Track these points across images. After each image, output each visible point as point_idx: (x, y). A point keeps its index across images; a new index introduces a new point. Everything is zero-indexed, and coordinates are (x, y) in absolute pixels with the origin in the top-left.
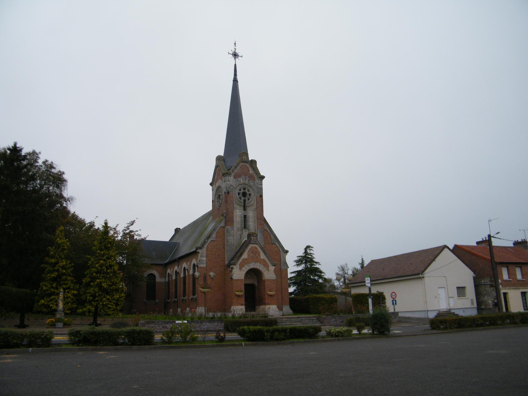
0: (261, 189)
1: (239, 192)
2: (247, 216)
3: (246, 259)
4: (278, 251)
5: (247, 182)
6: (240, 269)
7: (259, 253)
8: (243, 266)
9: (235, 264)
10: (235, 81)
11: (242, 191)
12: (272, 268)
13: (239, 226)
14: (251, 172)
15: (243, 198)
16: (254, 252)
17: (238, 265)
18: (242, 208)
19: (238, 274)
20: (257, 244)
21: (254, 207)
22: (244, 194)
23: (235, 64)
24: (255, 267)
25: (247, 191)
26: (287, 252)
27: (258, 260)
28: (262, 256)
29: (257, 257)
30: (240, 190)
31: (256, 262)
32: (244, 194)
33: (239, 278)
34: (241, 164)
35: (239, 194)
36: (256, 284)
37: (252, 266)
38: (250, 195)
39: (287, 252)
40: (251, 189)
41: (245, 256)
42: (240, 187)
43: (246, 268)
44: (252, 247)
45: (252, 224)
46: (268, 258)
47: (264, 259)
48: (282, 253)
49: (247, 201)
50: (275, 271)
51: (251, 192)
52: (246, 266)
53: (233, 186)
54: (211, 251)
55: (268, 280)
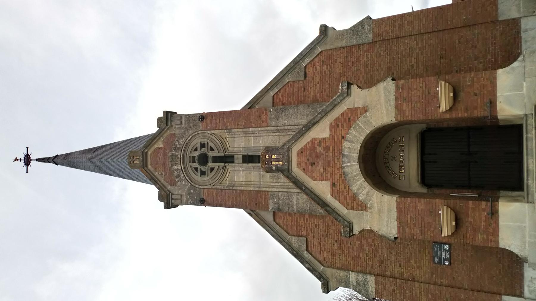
0: (189, 116)
1: (199, 174)
2: (245, 154)
3: (333, 185)
4: (322, 58)
5: (178, 154)
6: (363, 207)
7: (313, 141)
8: (354, 197)
9: (350, 226)
10: (55, 160)
11: (196, 165)
12: (358, 97)
14: (160, 144)
15: (211, 164)
17: (351, 215)
18: (229, 166)
19: (380, 214)
20: (289, 150)
21: (225, 134)
22: (203, 159)
24: (356, 155)
25: (196, 154)
26: (324, 30)
27: (334, 146)
28: (322, 131)
29: (327, 148)
30: (196, 169)
31: (340, 153)
33: (394, 214)
34: (150, 167)
35: (203, 173)
36: (416, 130)
37: (353, 167)
38: (203, 146)
39: (324, 30)
40: (193, 143)
41: (323, 189)
43: (361, 186)
44: (299, 165)
45: (260, 141)
46: (326, 113)
47: (332, 127)
48: (329, 45)
49: (216, 153)
50: (369, 83)
51: (196, 142)
52: (355, 188)
53: (189, 190)
54: (334, 255)
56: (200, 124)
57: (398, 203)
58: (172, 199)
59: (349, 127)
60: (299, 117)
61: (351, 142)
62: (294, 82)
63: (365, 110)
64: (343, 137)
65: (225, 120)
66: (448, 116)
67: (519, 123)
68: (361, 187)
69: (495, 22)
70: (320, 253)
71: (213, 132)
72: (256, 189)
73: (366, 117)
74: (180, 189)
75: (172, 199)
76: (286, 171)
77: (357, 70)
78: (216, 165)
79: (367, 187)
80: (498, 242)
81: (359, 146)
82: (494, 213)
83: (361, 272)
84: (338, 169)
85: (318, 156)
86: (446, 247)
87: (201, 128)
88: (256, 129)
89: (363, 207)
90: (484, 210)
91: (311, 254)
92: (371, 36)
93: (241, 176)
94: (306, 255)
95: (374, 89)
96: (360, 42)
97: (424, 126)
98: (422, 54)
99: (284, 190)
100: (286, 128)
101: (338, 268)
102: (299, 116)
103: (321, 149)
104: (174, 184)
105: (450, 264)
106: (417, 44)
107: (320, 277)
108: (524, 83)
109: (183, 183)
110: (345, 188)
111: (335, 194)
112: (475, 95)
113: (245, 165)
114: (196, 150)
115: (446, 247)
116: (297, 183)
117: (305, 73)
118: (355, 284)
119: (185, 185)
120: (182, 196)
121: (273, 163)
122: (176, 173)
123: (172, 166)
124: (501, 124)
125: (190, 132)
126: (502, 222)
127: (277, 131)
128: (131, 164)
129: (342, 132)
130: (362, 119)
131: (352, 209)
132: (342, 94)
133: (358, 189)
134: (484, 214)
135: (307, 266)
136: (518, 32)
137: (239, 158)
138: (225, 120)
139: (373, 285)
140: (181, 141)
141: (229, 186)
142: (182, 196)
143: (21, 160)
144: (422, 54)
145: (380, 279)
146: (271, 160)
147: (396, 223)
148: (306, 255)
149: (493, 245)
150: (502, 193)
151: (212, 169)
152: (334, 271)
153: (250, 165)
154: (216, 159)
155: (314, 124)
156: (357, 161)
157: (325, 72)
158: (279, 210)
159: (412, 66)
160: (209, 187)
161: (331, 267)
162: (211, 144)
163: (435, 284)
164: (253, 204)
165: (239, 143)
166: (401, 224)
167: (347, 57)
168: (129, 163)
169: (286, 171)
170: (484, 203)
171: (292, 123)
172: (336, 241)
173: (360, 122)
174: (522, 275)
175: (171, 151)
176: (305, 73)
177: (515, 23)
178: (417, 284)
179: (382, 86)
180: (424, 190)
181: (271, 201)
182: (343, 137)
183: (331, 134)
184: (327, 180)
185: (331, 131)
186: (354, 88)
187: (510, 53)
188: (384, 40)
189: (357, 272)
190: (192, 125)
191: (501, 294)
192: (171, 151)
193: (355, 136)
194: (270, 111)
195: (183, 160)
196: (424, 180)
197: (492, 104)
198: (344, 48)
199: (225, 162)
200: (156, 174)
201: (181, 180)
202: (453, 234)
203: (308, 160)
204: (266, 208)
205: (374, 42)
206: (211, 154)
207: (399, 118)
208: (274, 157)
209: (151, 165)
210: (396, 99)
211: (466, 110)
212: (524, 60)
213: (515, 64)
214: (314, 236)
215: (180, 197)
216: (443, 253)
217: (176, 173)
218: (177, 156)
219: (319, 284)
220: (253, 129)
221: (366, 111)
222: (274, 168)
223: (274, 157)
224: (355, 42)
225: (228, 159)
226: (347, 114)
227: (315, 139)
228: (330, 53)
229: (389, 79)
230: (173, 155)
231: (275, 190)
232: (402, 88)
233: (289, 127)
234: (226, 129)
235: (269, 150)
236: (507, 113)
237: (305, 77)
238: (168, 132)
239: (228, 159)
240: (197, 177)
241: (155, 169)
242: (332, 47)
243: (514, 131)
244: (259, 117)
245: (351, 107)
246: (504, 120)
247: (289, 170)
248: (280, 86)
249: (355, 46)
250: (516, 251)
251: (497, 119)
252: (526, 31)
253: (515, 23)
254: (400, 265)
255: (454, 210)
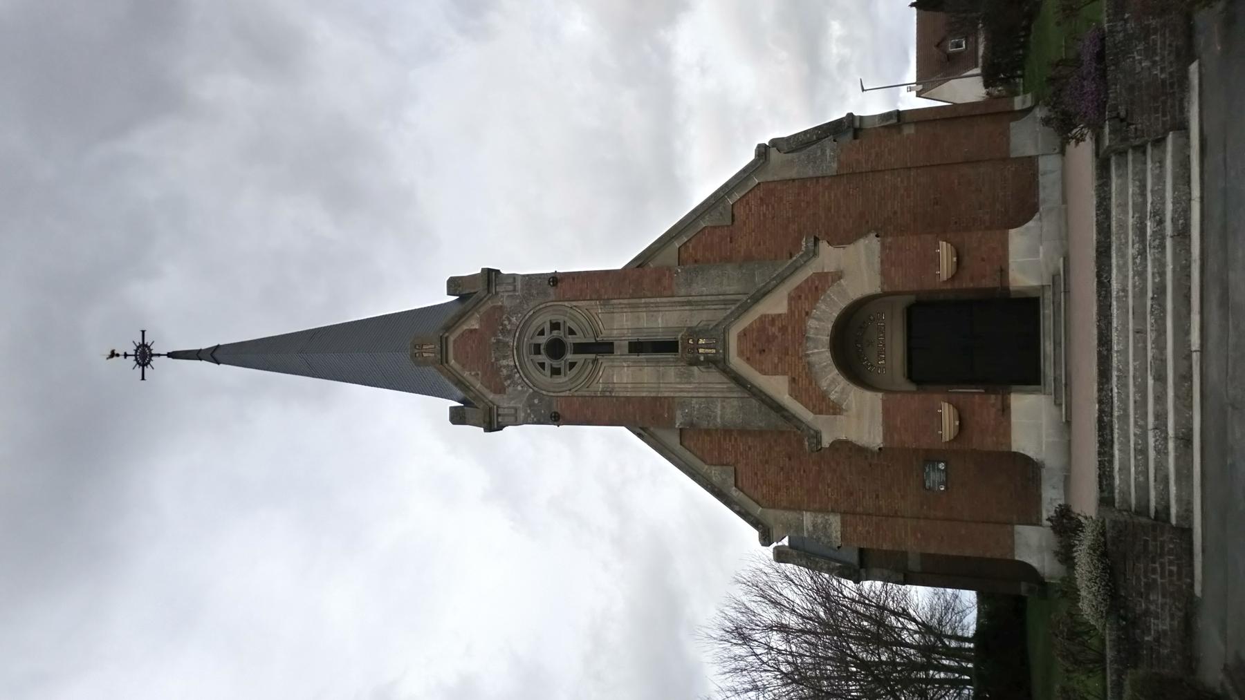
0: (529, 279)
1: (548, 372)
2: (634, 338)
3: (793, 380)
4: (760, 193)
5: (509, 339)
6: (835, 409)
7: (763, 318)
8: (824, 396)
9: (817, 436)
10: (215, 355)
11: (543, 358)
12: (829, 257)
13: (671, 373)
15: (570, 357)
16: (761, 343)
18: (604, 360)
19: (861, 418)
20: (725, 331)
21: (598, 310)
22: (556, 349)
23: (170, 355)
24: (826, 339)
25: (543, 340)
28: (776, 305)
29: (783, 329)
30: (542, 365)
31: (802, 336)
32: (556, 349)
33: (879, 418)
34: (452, 362)
35: (556, 372)
36: (902, 303)
37: (821, 355)
38: (555, 326)
41: (777, 387)
42: (530, 367)
43: (833, 381)
44: (741, 353)
45: (662, 320)
46: (782, 279)
49: (579, 338)
50: (842, 239)
51: (544, 320)
52: (824, 385)
53: (532, 397)
55: (884, 274)
56: (551, 290)
57: (884, 401)
58: (498, 415)
59: (816, 300)
60: (730, 283)
61: (818, 319)
62: (715, 227)
63: (838, 275)
64: (807, 314)
65: (597, 285)
66: (949, 287)
67: (1034, 295)
68: (833, 381)
69: (1006, 159)
70: (756, 488)
71: (574, 303)
72: (653, 395)
73: (839, 285)
74: (513, 399)
75: (498, 415)
76: (719, 363)
77: (814, 214)
78: (580, 358)
79: (842, 382)
80: (1010, 445)
81: (830, 326)
82: (1005, 410)
83: (820, 511)
84: (800, 358)
85: (770, 339)
86: (942, 466)
87: (552, 298)
88: (652, 300)
89: (835, 409)
90: (993, 405)
91: (742, 490)
92: (835, 165)
93: (625, 376)
94: (735, 493)
95: (851, 248)
96: (819, 174)
97: (912, 298)
98: (909, 196)
99: (700, 395)
100: (704, 298)
101: (785, 508)
102: (725, 281)
103: (774, 330)
104: (501, 390)
105: (947, 488)
106: (902, 182)
107: (755, 523)
108: (1041, 248)
109: (519, 388)
110: (810, 383)
111: (795, 394)
112: (983, 260)
113: (634, 357)
114: (542, 333)
115: (942, 466)
116: (738, 380)
117: (733, 215)
118: (811, 529)
119: (522, 392)
120: (516, 410)
121: (701, 351)
122: (505, 372)
123: (497, 360)
124: (1013, 296)
125: (532, 304)
126: (1014, 419)
127: (689, 303)
128: (418, 360)
129: (807, 307)
130: (835, 288)
131: (821, 413)
132: (806, 253)
133: (829, 385)
134: (993, 410)
135: (737, 508)
136: (1035, 175)
137: (622, 347)
138: (597, 285)
139: (839, 528)
140: (514, 319)
141: (603, 391)
142: (516, 410)
143: (126, 355)
144: (909, 196)
145: (849, 518)
146: (697, 346)
147: (881, 429)
148: (735, 493)
149: (1004, 448)
150: (1015, 387)
151: (572, 365)
152: (779, 513)
153: (642, 356)
154: (580, 348)
155: (765, 294)
156: (828, 346)
157: (764, 215)
158: (692, 425)
159: (895, 213)
160: (567, 393)
161: (774, 507)
162: (570, 324)
163: (926, 518)
164: (648, 420)
165: (622, 323)
166: (889, 429)
167: (799, 194)
168: (413, 356)
169: (719, 363)
170: (993, 396)
171: (714, 291)
172: (782, 469)
173: (832, 292)
174: (1040, 496)
175: (495, 335)
176: (733, 215)
177: (1031, 162)
178: (901, 521)
179: (862, 243)
180: (913, 387)
181: (678, 413)
182: (807, 314)
183: (790, 309)
184: (784, 373)
185: (790, 304)
186: (823, 245)
187: (1023, 208)
188: (854, 173)
189: (815, 511)
190: (535, 292)
191: (1012, 524)
192: (495, 335)
193: (824, 311)
194: (677, 272)
195: (502, 351)
196: (911, 376)
197: (1003, 271)
198: (794, 180)
199: (597, 353)
200: (466, 374)
201: (515, 384)
202: (955, 438)
203: (754, 345)
204: (670, 424)
205: (839, 176)
206: (570, 340)
207: (886, 288)
208: (701, 342)
209: (455, 359)
210: (882, 262)
211: (972, 279)
212: (1040, 219)
213: (1031, 224)
214: (747, 464)
215: (513, 411)
216: (938, 475)
217: (505, 372)
218: (506, 345)
219: (754, 534)
220: (647, 300)
221: (840, 278)
222: (702, 358)
223: (701, 342)
224: (811, 174)
225: (605, 348)
226: (813, 282)
227: (765, 316)
228: (772, 186)
229: (873, 235)
230: (498, 341)
231: (686, 394)
232: (890, 248)
233: (709, 298)
234: (599, 299)
235: (694, 333)
236: (1022, 284)
237: (733, 220)
238: (490, 304)
239: (605, 348)
240: (544, 378)
241: (463, 366)
242: (776, 178)
243: (1028, 305)
244: (659, 281)
245: (820, 271)
246: (1018, 292)
247: (725, 360)
248: (691, 234)
249: (811, 178)
250: (1031, 454)
251: (1007, 289)
252: (1045, 173)
253: (1031, 162)
254: (877, 496)
255: (956, 407)
